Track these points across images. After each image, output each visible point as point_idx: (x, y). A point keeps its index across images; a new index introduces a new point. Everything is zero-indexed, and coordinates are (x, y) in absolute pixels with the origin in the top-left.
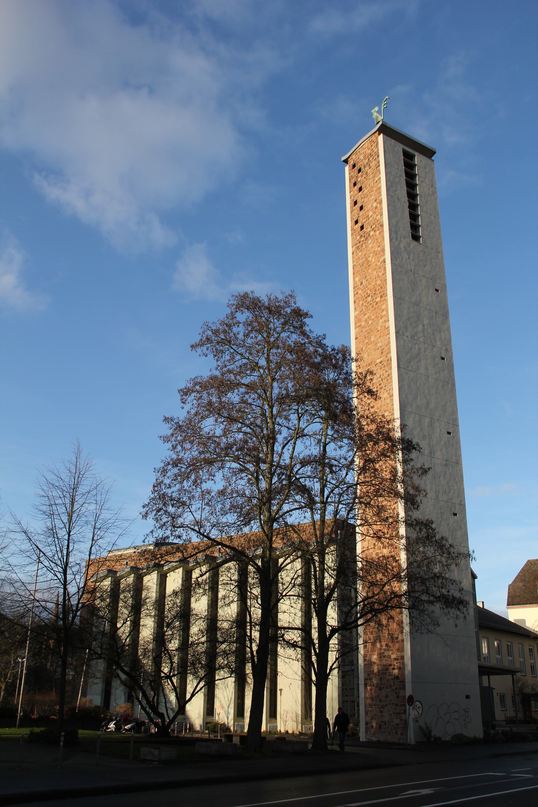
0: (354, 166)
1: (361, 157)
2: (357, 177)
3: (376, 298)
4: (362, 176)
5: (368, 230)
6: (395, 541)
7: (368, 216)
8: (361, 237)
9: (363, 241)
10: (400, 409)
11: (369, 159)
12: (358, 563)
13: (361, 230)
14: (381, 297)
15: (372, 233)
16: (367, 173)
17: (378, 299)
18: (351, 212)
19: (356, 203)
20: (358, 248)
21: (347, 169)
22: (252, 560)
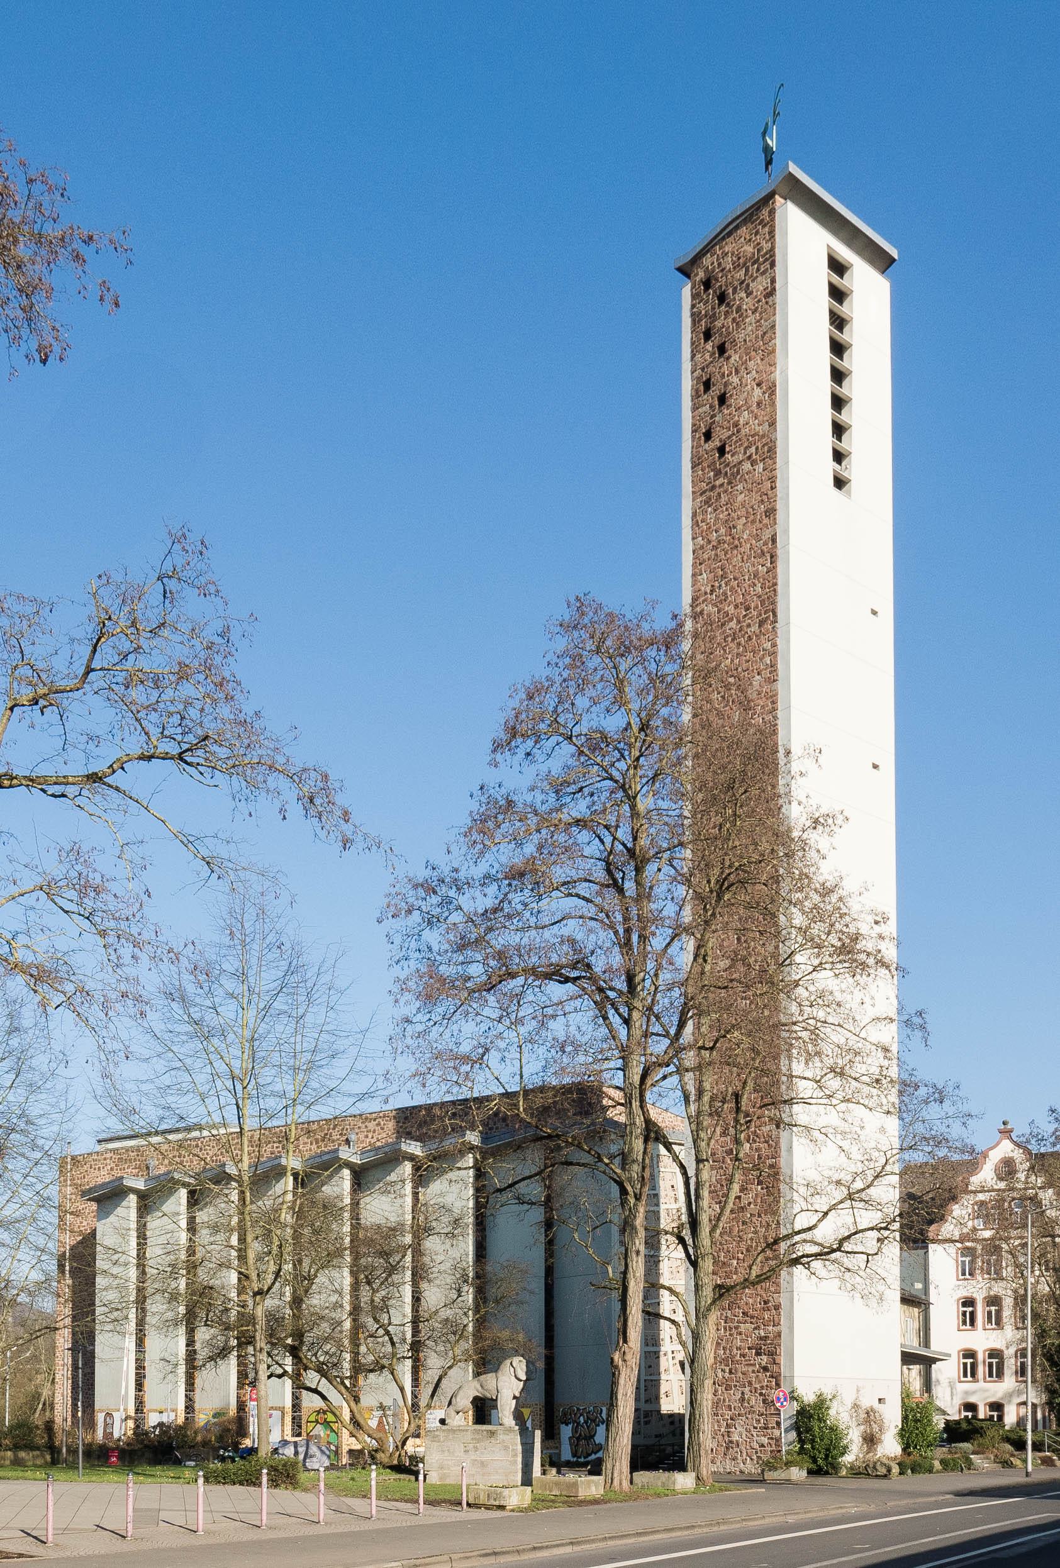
0: (707, 284)
1: (728, 263)
2: (714, 318)
3: (749, 626)
4: (727, 313)
5: (736, 459)
6: (475, 1005)
7: (736, 425)
8: (718, 473)
9: (722, 485)
10: (829, 206)
11: (747, 270)
12: (663, 1292)
13: (709, 380)
14: (761, 624)
15: (747, 466)
16: (739, 309)
17: (755, 628)
18: (695, 408)
19: (707, 385)
20: (707, 502)
21: (687, 292)
22: (974, 1230)
